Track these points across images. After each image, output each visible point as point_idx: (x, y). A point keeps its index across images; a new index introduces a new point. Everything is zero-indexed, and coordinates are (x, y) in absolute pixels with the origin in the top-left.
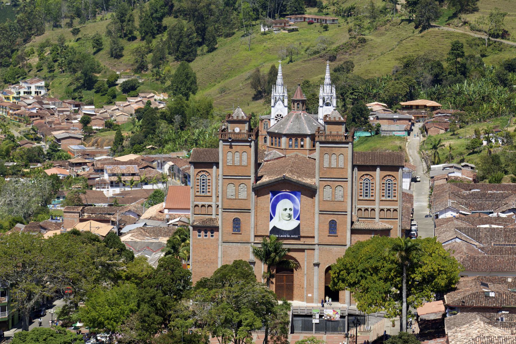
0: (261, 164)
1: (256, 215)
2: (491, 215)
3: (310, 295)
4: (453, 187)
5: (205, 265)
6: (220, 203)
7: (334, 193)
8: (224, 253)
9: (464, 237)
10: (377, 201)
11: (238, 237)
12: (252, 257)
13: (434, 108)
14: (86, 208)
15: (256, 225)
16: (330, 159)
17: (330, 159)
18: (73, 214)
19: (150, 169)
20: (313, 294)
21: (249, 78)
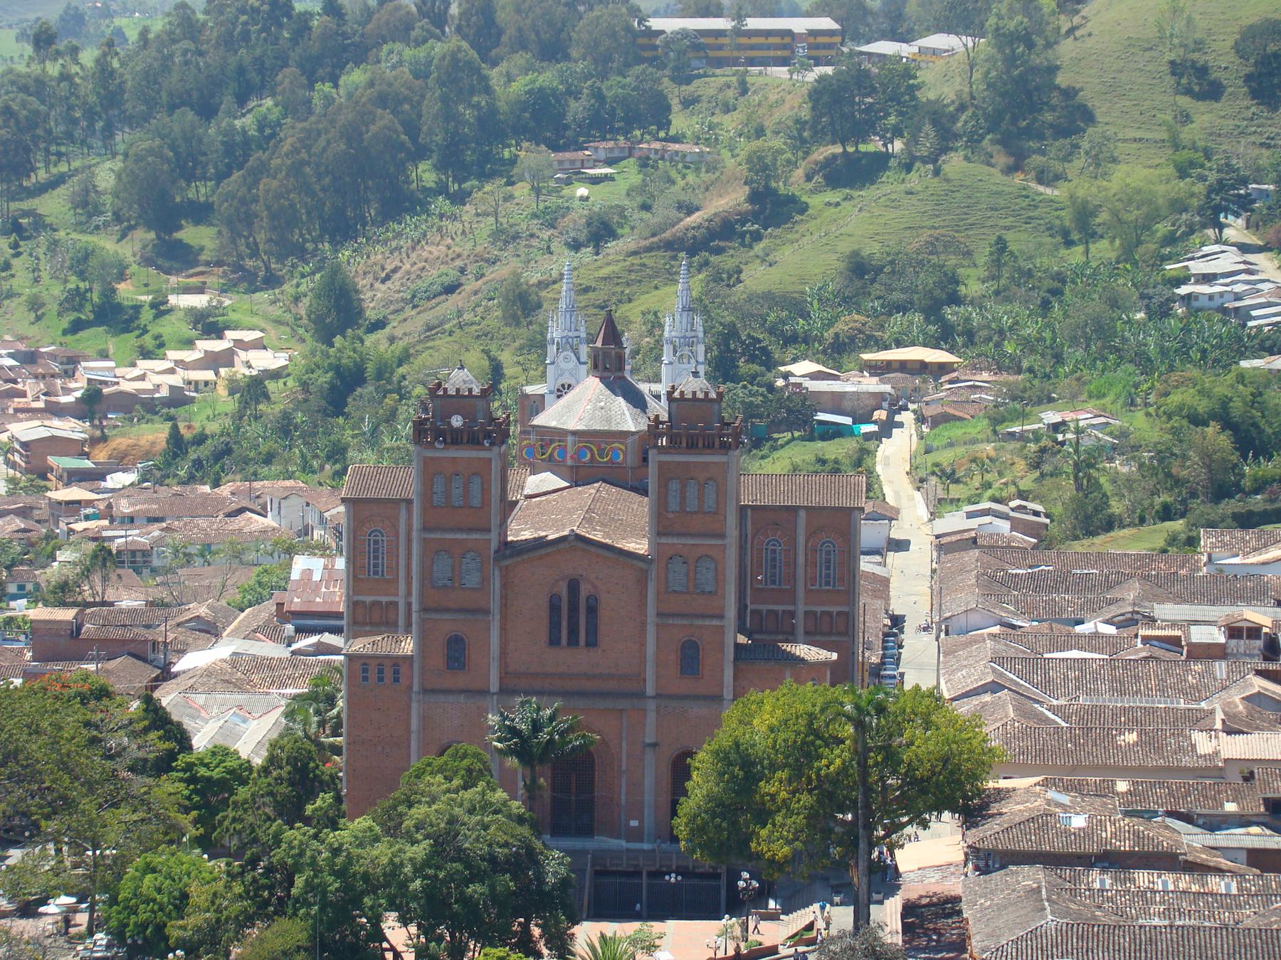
0: (517, 502)
1: (503, 629)
2: (1079, 629)
3: (634, 823)
4: (986, 558)
5: (379, 749)
6: (414, 599)
7: (691, 575)
8: (425, 720)
9: (1012, 680)
10: (801, 593)
11: (461, 680)
12: (815, 201)
13: (943, 368)
14: (88, 611)
15: (503, 653)
16: (683, 492)
17: (683, 492)
18: (544, 498)
19: (249, 514)
20: (641, 822)
21: (993, 816)
